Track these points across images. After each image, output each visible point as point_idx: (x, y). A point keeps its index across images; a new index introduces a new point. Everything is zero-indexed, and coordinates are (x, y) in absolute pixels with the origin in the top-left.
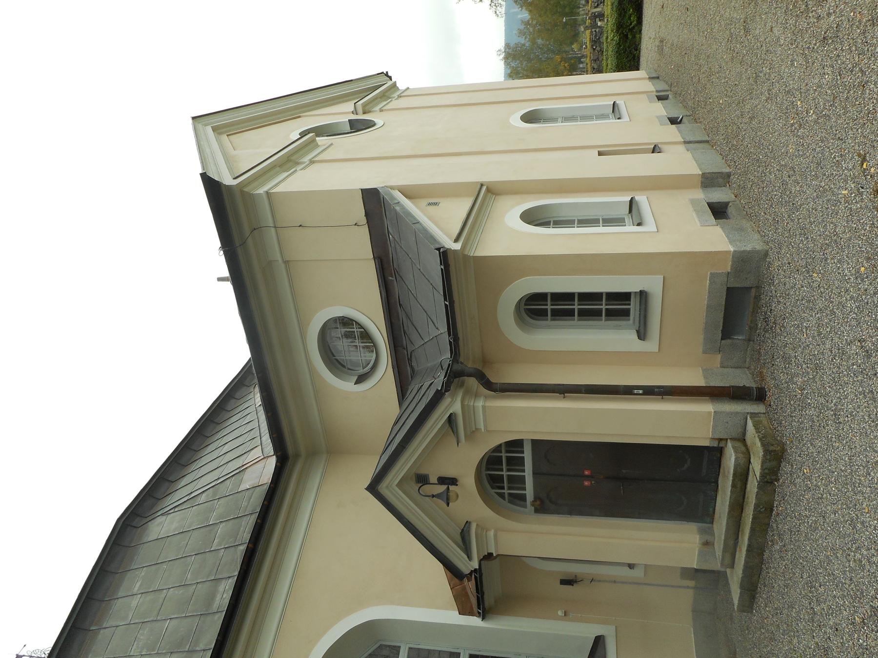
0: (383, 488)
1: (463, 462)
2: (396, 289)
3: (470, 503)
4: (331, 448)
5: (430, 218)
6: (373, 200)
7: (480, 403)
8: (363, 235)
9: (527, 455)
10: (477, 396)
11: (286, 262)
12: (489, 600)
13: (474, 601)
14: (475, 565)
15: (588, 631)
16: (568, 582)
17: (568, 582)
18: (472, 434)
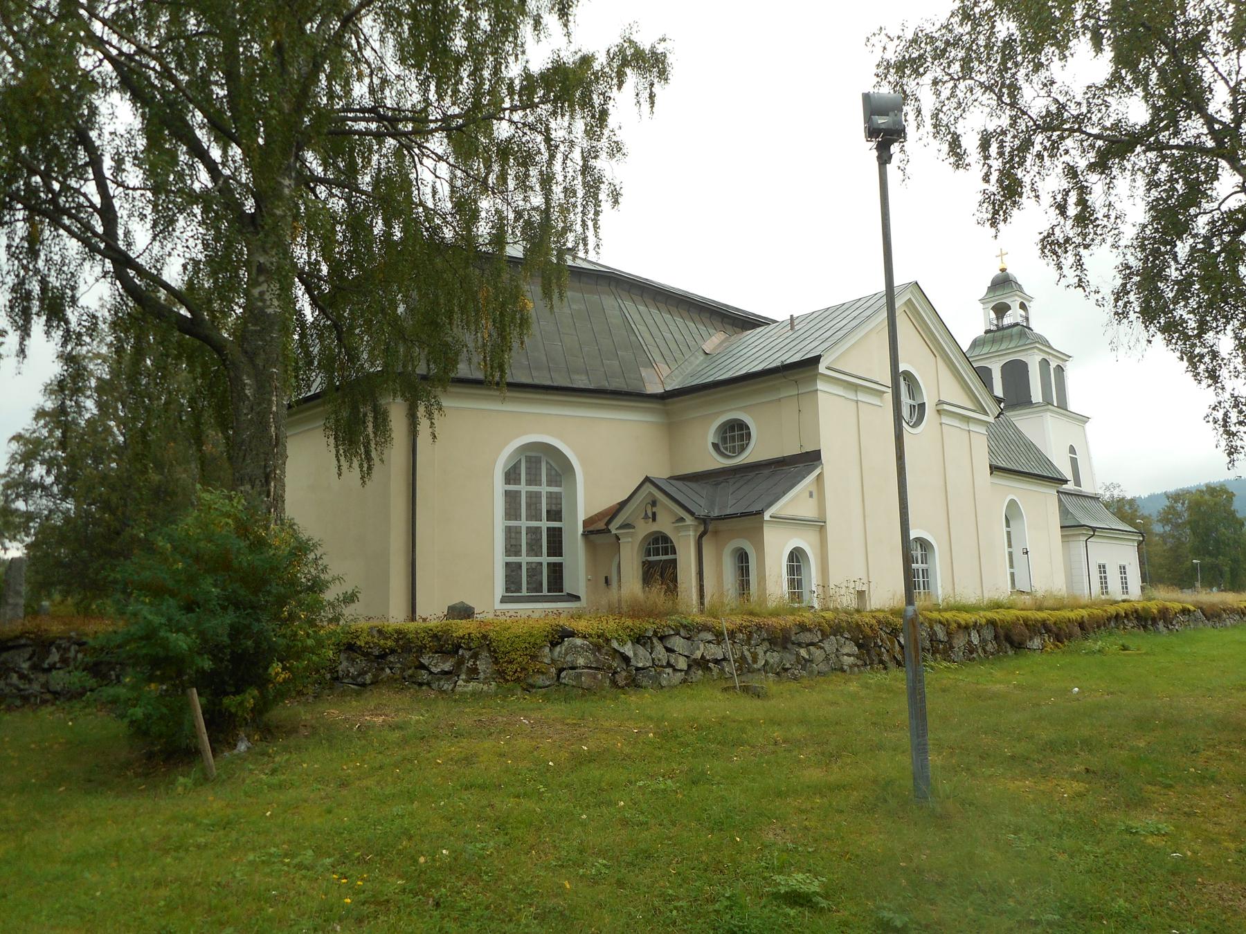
0: (648, 484)
1: (664, 525)
2: (766, 472)
3: (644, 529)
4: (672, 430)
5: (797, 496)
6: (813, 458)
7: (692, 533)
8: (797, 451)
9: (670, 557)
10: (696, 531)
11: (779, 400)
12: (592, 537)
13: (591, 528)
14: (614, 532)
15: (582, 593)
16: (607, 581)
17: (607, 581)
18: (677, 529)
